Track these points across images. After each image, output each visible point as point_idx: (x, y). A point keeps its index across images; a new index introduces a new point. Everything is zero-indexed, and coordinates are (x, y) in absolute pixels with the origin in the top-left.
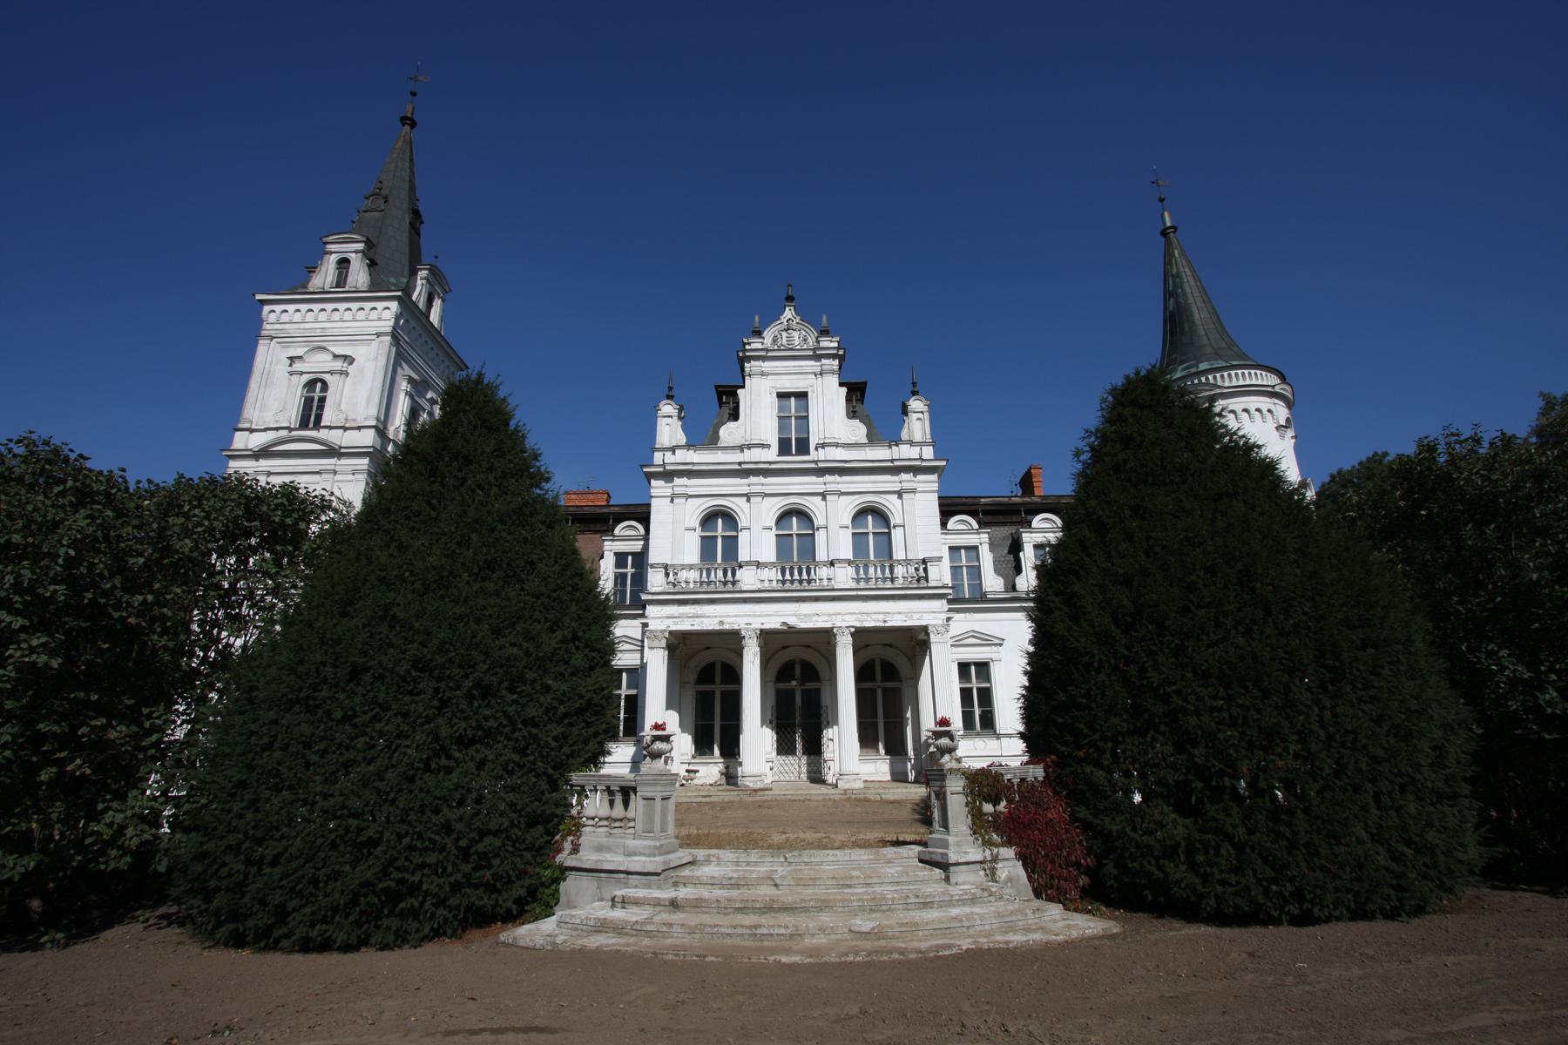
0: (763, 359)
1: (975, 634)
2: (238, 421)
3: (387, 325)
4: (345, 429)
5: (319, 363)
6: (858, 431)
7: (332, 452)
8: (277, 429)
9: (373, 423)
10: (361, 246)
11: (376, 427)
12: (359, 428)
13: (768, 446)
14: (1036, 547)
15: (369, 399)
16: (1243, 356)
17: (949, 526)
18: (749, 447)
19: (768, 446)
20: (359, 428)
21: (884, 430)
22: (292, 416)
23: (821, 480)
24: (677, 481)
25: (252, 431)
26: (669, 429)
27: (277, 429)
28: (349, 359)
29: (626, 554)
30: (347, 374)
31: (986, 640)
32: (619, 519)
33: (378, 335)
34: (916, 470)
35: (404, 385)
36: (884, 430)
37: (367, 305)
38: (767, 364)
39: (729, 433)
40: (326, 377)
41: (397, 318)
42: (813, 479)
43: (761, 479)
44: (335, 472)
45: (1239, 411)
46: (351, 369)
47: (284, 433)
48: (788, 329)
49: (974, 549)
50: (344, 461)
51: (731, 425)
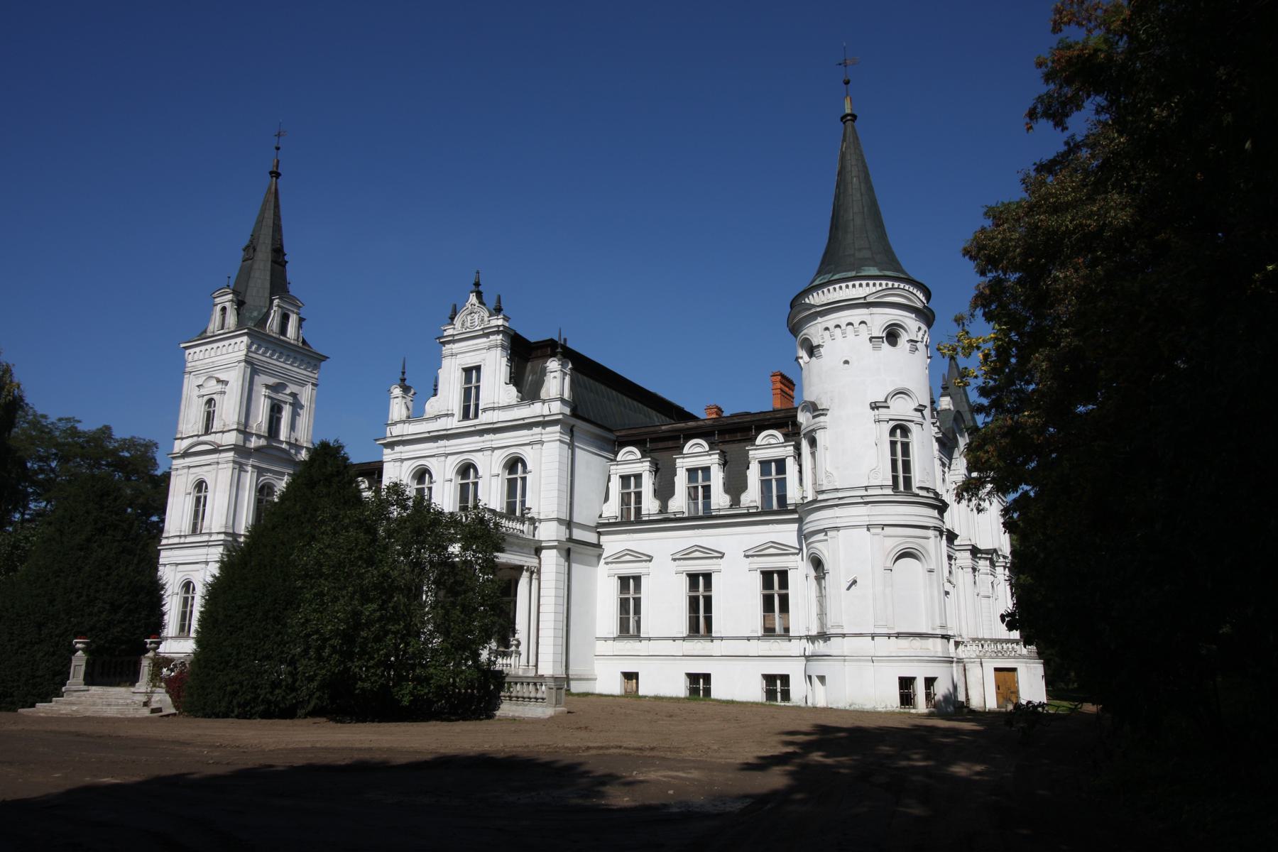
0: (454, 342)
1: (630, 552)
3: (241, 355)
4: (223, 432)
5: (212, 386)
6: (512, 393)
7: (216, 450)
10: (230, 297)
11: (237, 430)
13: (453, 415)
16: (898, 268)
18: (440, 417)
19: (453, 415)
23: (436, 445)
24: (397, 449)
25: (182, 439)
26: (398, 408)
28: (225, 383)
32: (761, 428)
33: (239, 362)
34: (544, 424)
37: (233, 341)
38: (457, 345)
39: (432, 406)
40: (214, 396)
41: (249, 347)
42: (477, 438)
43: (491, 436)
45: (832, 328)
46: (227, 389)
47: (195, 439)
48: (474, 316)
51: (433, 399)
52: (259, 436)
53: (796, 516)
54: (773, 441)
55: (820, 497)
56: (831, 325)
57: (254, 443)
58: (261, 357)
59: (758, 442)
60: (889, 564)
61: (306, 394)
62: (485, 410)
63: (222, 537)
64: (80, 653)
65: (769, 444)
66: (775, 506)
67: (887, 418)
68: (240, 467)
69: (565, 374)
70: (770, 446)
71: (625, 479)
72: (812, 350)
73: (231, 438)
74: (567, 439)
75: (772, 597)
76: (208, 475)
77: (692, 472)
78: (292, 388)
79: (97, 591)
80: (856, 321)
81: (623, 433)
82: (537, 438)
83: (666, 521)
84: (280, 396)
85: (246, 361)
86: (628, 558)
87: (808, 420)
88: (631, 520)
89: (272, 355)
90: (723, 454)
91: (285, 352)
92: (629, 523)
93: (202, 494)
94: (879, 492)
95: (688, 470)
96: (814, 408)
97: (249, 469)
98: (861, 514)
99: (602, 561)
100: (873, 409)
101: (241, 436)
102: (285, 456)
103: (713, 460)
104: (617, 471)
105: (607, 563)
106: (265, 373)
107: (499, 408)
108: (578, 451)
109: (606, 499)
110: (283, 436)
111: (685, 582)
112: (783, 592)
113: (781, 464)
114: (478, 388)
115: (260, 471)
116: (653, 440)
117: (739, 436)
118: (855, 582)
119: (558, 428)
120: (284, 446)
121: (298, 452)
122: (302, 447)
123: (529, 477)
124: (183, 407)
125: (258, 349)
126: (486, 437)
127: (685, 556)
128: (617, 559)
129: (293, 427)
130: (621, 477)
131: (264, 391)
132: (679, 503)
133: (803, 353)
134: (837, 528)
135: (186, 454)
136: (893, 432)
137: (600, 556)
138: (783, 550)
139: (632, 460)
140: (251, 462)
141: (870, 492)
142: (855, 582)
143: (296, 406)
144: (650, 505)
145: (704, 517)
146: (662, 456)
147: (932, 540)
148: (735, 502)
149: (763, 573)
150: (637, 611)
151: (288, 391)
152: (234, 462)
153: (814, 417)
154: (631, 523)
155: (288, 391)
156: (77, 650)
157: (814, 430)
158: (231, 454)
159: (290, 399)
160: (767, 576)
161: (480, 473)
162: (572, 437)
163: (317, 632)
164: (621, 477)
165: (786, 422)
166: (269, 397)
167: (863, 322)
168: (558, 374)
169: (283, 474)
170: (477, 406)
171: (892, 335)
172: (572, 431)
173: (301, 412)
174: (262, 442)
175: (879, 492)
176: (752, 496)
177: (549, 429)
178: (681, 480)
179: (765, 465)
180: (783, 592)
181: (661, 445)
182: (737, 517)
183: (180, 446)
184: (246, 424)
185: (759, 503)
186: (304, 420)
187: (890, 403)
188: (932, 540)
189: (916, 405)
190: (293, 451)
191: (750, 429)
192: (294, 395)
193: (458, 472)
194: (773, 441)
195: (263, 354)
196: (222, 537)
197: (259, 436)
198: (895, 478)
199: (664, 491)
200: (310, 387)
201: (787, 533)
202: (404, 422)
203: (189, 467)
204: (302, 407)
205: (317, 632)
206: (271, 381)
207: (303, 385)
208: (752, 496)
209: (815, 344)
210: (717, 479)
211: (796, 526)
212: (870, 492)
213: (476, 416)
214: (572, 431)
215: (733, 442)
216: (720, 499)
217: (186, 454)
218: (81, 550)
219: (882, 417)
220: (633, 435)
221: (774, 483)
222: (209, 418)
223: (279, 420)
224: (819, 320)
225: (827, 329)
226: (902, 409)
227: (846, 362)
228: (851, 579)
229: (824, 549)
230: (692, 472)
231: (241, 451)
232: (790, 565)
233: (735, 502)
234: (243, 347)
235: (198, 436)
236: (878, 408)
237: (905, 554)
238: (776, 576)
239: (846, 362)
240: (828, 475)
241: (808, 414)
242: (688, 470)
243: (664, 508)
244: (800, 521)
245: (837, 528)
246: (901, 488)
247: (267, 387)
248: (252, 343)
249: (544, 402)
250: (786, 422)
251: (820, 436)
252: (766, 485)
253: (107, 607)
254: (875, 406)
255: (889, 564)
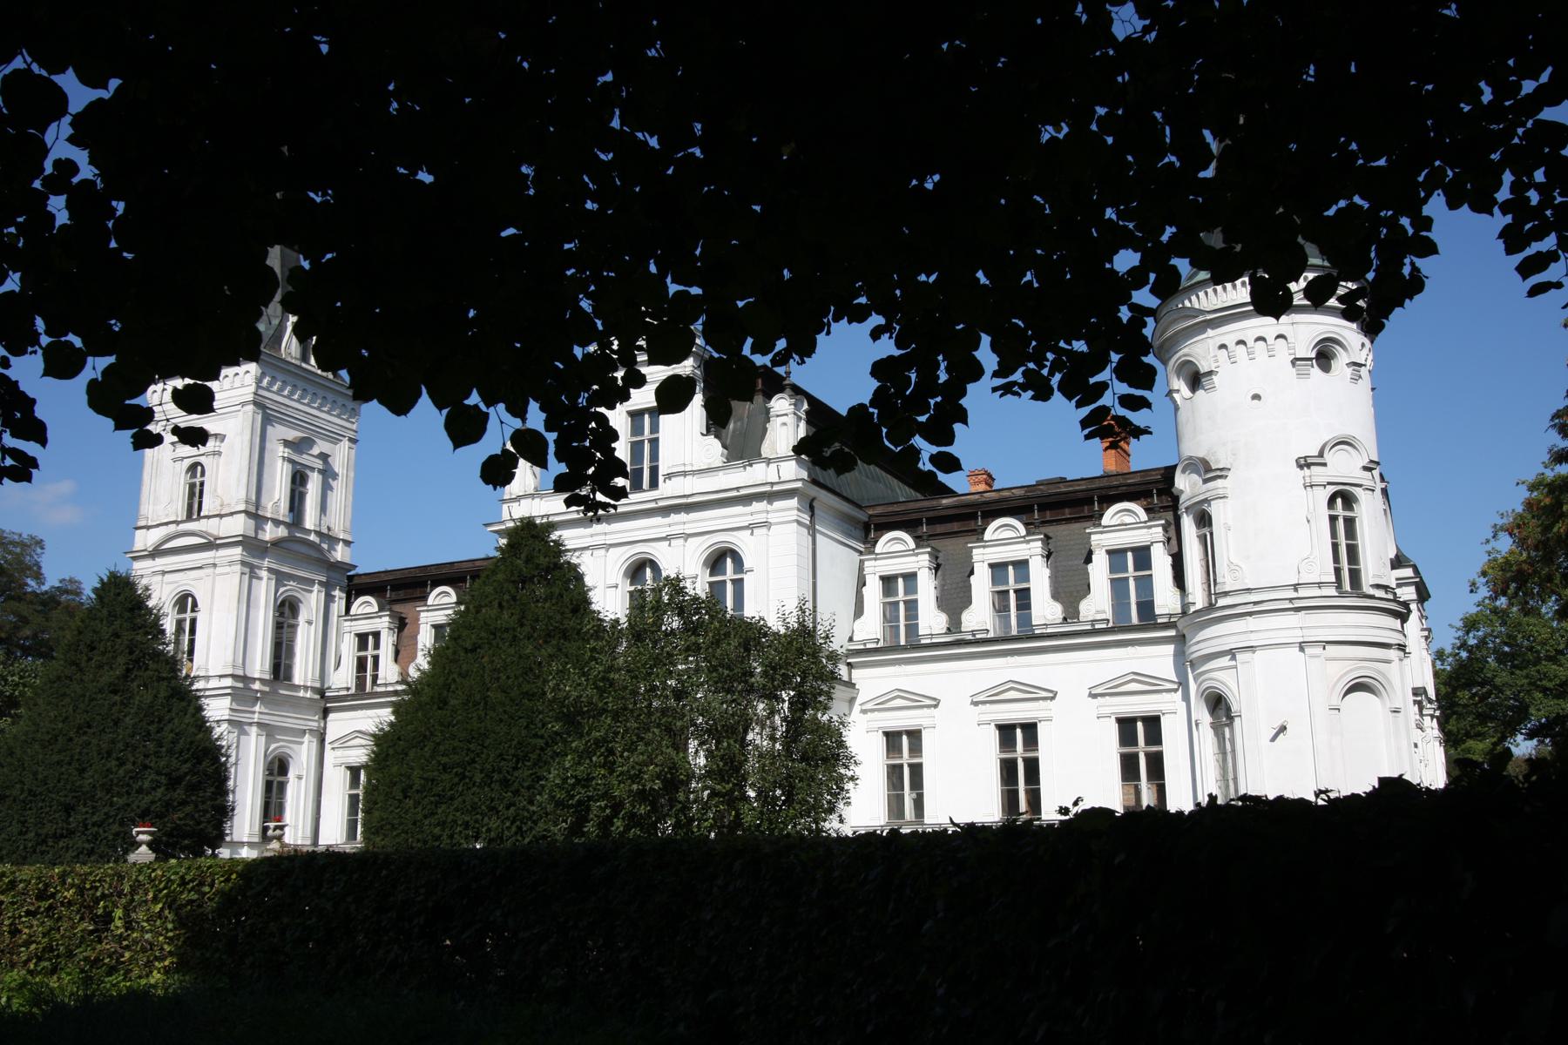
1: (902, 693)
2: (137, 519)
3: (248, 393)
4: (221, 516)
6: (713, 449)
7: (211, 545)
8: (167, 524)
9: (242, 507)
11: (245, 512)
12: (232, 514)
14: (435, 627)
15: (239, 480)
17: (353, 611)
20: (232, 514)
21: (744, 449)
22: (179, 510)
23: (748, 509)
25: (148, 528)
27: (167, 524)
29: (367, 635)
30: (219, 453)
31: (1033, 693)
32: (436, 584)
33: (243, 404)
34: (771, 497)
35: (278, 452)
36: (744, 449)
41: (259, 381)
42: (658, 520)
43: (682, 517)
44: (215, 565)
46: (224, 447)
47: (172, 528)
49: (1022, 565)
50: (222, 552)
52: (277, 523)
53: (1172, 633)
54: (1128, 519)
55: (1222, 602)
56: (1230, 341)
57: (270, 533)
58: (279, 396)
59: (1105, 520)
60: (1336, 701)
61: (341, 456)
62: (669, 476)
63: (228, 682)
64: (144, 848)
65: (1124, 524)
66: (1135, 620)
67: (1324, 480)
68: (251, 571)
69: (799, 418)
70: (1124, 527)
71: (888, 581)
72: (1196, 380)
73: (237, 526)
74: (806, 518)
75: (1135, 756)
76: (198, 585)
77: (998, 568)
78: (321, 446)
79: (146, 756)
80: (1249, 338)
81: (879, 510)
82: (761, 518)
83: (959, 644)
84: (304, 459)
85: (255, 403)
86: (899, 702)
87: (1193, 485)
88: (901, 644)
89: (292, 393)
90: (934, 556)
91: (311, 389)
92: (896, 648)
93: (188, 615)
94: (1316, 592)
95: (991, 566)
96: (1206, 469)
97: (264, 574)
98: (1290, 626)
99: (857, 708)
100: (1301, 467)
101: (252, 523)
102: (314, 554)
103: (1032, 550)
104: (876, 569)
105: (864, 712)
106: (282, 422)
107: (694, 473)
108: (818, 536)
109: (859, 611)
110: (310, 520)
111: (993, 736)
112: (1154, 749)
113: (1142, 556)
114: (654, 443)
115: (281, 579)
116: (931, 521)
117: (1067, 513)
118: (1283, 729)
119: (794, 502)
120: (312, 537)
121: (332, 548)
122: (338, 540)
123: (748, 579)
124: (146, 477)
125: (271, 384)
126: (674, 518)
127: (994, 697)
128: (882, 704)
129: (323, 508)
130: (882, 578)
131: (281, 451)
132: (979, 616)
133: (1180, 386)
134: (1251, 648)
135: (156, 553)
136: (1331, 502)
137: (852, 701)
138: (1152, 685)
139: (898, 551)
140: (266, 563)
141: (1302, 593)
142: (1283, 729)
143: (328, 474)
144: (932, 621)
145: (1020, 636)
146: (948, 546)
147: (1396, 664)
148: (1071, 614)
149: (1120, 721)
150: (917, 783)
151: (316, 451)
152: (243, 563)
153: (1206, 481)
154: (904, 649)
155: (316, 451)
156: (139, 844)
157: (1206, 501)
158: (239, 550)
159: (319, 464)
160: (1126, 726)
161: (747, 565)
162: (812, 516)
163: (606, 795)
164: (882, 578)
165: (1156, 491)
166: (290, 461)
167: (1279, 336)
168: (790, 419)
169: (312, 582)
170: (654, 471)
171: (1324, 355)
172: (812, 508)
173: (334, 484)
174: (282, 532)
175: (1316, 592)
176: (1097, 604)
177: (778, 504)
178: (981, 583)
179: (1116, 555)
180: (1154, 749)
181: (940, 529)
182: (1075, 636)
183: (145, 540)
184: (258, 505)
185: (1109, 615)
186: (340, 496)
187: (1328, 457)
188: (1396, 664)
189: (1365, 462)
190: (325, 546)
191: (1090, 501)
192: (324, 457)
193: (626, 574)
194: (1128, 519)
195: (279, 392)
196: (228, 682)
197: (277, 523)
198: (1338, 571)
199: (954, 599)
200: (345, 444)
201: (1158, 659)
202: (532, 496)
203: (164, 573)
204: (335, 476)
205: (606, 795)
206: (292, 434)
207: (335, 441)
208: (1097, 604)
209: (1203, 368)
210: (1040, 578)
211: (1170, 649)
212: (1302, 593)
213: (654, 484)
214: (812, 508)
215: (1058, 522)
216: (1045, 610)
217: (156, 553)
218: (115, 692)
219: (1316, 480)
220: (897, 513)
221: (1132, 583)
222: (195, 495)
223: (302, 496)
224: (1210, 332)
225: (1223, 346)
226: (1345, 467)
227: (1256, 397)
228: (1277, 725)
229: (1223, 677)
230: (998, 568)
231: (251, 545)
232: (1163, 707)
233: (1071, 614)
234: (250, 380)
235: (177, 523)
236: (1309, 466)
237: (1357, 687)
238: (1140, 725)
239: (1256, 397)
240: (1233, 568)
241: (1195, 477)
242: (991, 566)
243: (955, 625)
244: (1181, 640)
245: (1251, 648)
246: (1347, 586)
247: (287, 443)
248: (263, 375)
249: (768, 461)
250: (1156, 491)
251: (1215, 510)
252: (1118, 587)
253: (163, 780)
254: (1304, 463)
255: (1336, 701)
